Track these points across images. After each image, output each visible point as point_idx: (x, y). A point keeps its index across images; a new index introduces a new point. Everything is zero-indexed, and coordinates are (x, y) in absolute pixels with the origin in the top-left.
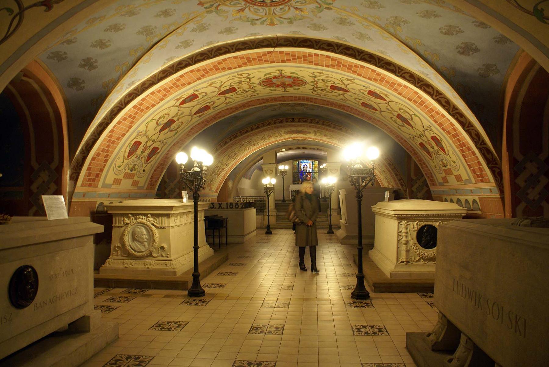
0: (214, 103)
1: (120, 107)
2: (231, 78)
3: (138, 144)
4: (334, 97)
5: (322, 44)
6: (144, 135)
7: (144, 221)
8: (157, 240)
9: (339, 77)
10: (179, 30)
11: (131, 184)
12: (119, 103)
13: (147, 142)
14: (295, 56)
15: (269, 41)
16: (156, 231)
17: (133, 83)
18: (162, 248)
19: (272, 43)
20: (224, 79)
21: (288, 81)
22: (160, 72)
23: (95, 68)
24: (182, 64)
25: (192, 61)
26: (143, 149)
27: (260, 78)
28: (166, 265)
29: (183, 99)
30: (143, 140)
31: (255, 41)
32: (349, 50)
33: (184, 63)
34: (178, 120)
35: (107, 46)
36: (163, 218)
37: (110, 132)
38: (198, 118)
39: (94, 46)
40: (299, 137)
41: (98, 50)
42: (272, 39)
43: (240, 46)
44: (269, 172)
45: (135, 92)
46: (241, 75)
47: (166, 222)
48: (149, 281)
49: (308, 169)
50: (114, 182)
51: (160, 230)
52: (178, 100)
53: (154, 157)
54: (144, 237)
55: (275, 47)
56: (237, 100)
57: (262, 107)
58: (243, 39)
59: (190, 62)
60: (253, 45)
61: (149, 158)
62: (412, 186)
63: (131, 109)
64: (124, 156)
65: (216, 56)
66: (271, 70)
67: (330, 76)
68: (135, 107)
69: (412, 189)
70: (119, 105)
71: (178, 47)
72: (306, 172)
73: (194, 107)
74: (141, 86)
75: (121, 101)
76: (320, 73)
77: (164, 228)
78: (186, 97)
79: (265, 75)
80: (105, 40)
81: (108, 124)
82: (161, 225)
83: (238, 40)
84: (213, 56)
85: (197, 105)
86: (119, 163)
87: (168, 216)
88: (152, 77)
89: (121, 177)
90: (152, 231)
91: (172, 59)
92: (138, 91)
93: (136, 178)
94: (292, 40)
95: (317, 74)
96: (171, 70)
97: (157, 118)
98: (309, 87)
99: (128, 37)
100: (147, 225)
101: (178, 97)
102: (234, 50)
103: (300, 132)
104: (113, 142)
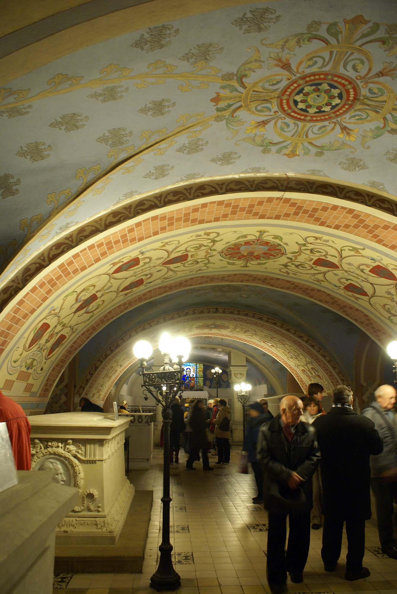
0: (151, 275)
1: (40, 264)
2: (194, 238)
3: (46, 326)
4: (307, 277)
5: (348, 192)
6: (56, 315)
7: (60, 451)
8: (81, 483)
9: (339, 244)
10: (163, 145)
11: (23, 389)
12: (39, 258)
13: (56, 327)
14: (52, 280)
15: (274, 182)
16: (80, 468)
17: (67, 226)
18: (90, 496)
19: (279, 185)
20: (183, 239)
21: (260, 250)
22: (109, 215)
23: (13, 194)
24: (144, 204)
25: (160, 201)
26: (49, 337)
27: (228, 243)
28: (96, 525)
29: (121, 264)
30: (52, 322)
31: (254, 181)
32: (384, 203)
33: (148, 204)
34: (100, 297)
35: (43, 158)
36: (92, 446)
37: (17, 304)
38: (122, 298)
39: (22, 154)
40: (211, 334)
41: (27, 163)
42: (279, 179)
43: (232, 186)
44: (239, 376)
45: (67, 241)
46: (208, 234)
47: (97, 453)
48: (72, 558)
49: (192, 373)
50: (4, 386)
51: (86, 465)
52: (114, 264)
53: (57, 349)
54: (59, 477)
55: (285, 191)
56: (179, 274)
57: (188, 291)
58: (237, 176)
59: (157, 202)
60: (252, 186)
61: (52, 350)
62: (363, 394)
63: (56, 269)
64: (25, 345)
65: (198, 197)
66: (248, 229)
67: (330, 243)
68: (61, 266)
69: (363, 398)
70: (39, 261)
71: (148, 175)
72: (189, 377)
73: (127, 278)
74: (78, 234)
75: (42, 254)
76: (316, 238)
77: (94, 462)
78: (125, 261)
79: (238, 238)
80: (44, 144)
81: (17, 290)
82: (88, 458)
83: (230, 177)
84: (192, 197)
85: (132, 276)
86: (16, 355)
87: (101, 442)
88: (95, 221)
89: (14, 378)
90: (73, 467)
91: (131, 194)
92: (72, 241)
93: (31, 381)
94: (306, 183)
95: (310, 240)
96: (127, 213)
97: (79, 290)
98: (283, 260)
99: (80, 148)
100: (65, 458)
101: (117, 260)
102: (224, 190)
103: (217, 327)
104: (17, 321)
